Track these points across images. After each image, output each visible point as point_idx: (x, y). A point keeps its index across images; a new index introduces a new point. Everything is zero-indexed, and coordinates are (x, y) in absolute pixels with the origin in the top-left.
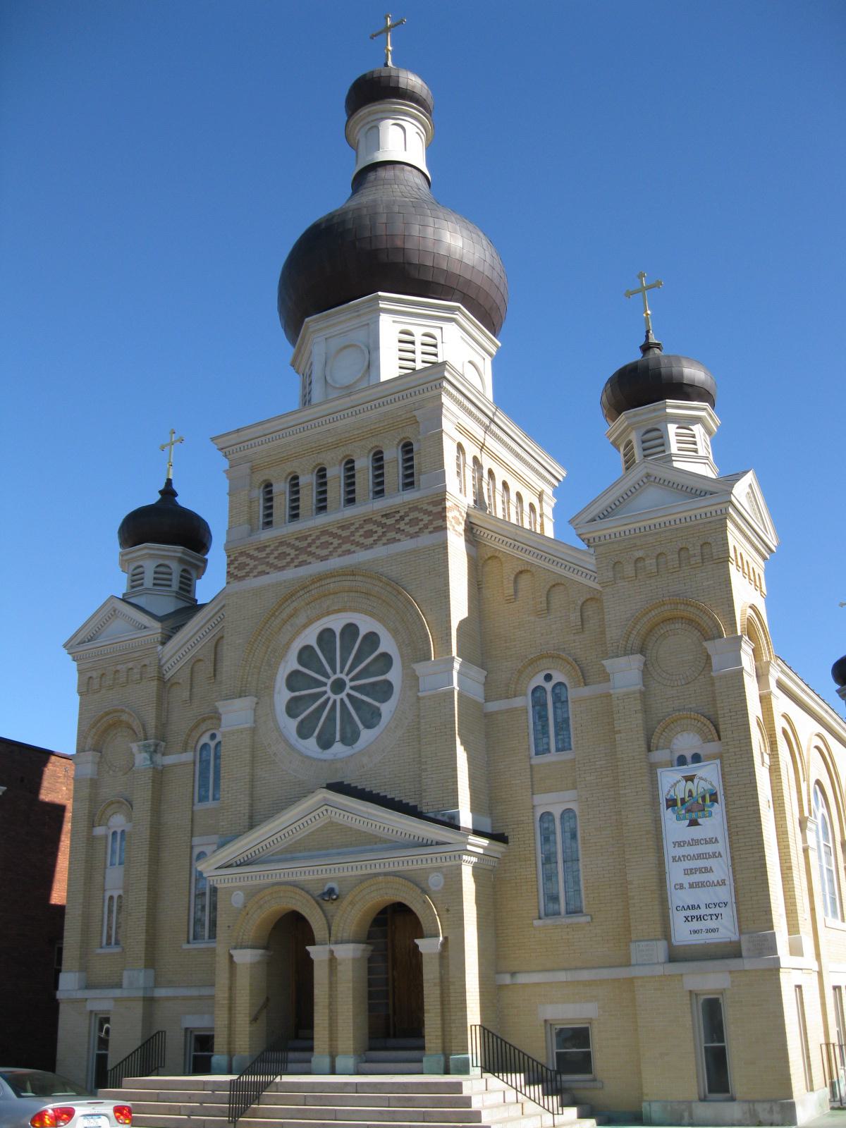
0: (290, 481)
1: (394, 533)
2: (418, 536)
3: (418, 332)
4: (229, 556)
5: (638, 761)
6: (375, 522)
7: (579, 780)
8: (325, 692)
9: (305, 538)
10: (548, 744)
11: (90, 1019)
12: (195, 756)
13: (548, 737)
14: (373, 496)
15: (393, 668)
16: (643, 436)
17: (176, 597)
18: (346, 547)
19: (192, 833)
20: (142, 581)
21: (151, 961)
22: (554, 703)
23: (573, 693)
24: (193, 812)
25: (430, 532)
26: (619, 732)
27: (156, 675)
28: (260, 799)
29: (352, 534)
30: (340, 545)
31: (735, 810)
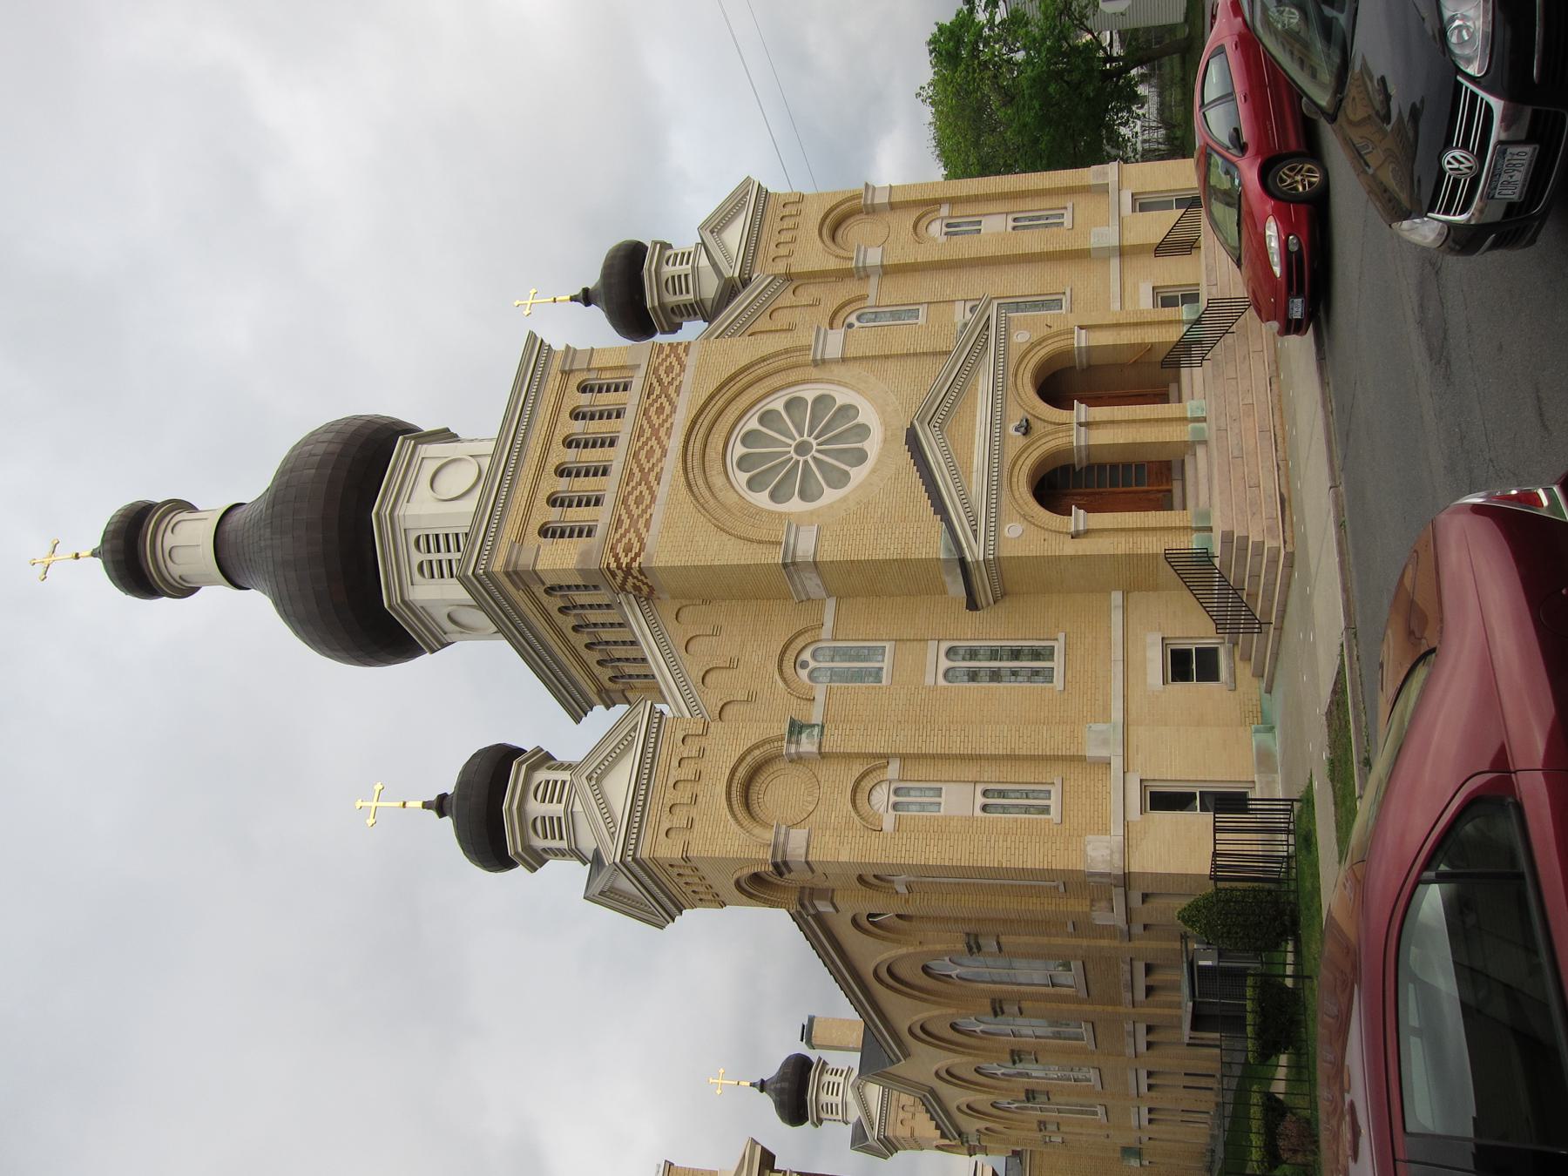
3: (417, 557)
16: (538, 836)
20: (547, 819)
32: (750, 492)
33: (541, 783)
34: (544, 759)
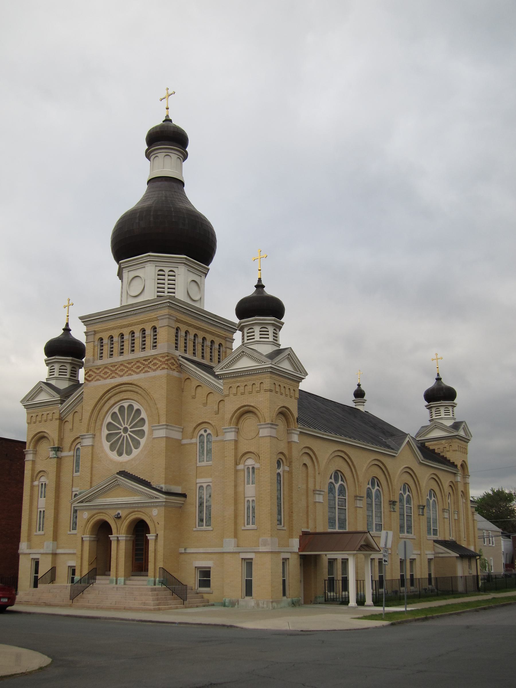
0: (110, 339)
1: (147, 368)
2: (156, 371)
3: (167, 270)
4: (85, 371)
5: (231, 469)
6: (141, 363)
7: (213, 474)
8: (120, 433)
9: (114, 366)
10: (204, 458)
11: (32, 562)
12: (74, 453)
13: (204, 456)
14: (141, 350)
15: (145, 425)
17: (69, 380)
18: (130, 372)
19: (72, 486)
21: (55, 538)
22: (207, 442)
23: (214, 438)
24: (73, 477)
25: (161, 370)
26: (226, 457)
27: (58, 417)
28: (95, 476)
29: (132, 367)
30: (127, 371)
31: (262, 491)
32: (111, 414)
33: (268, 329)
34: (278, 327)
